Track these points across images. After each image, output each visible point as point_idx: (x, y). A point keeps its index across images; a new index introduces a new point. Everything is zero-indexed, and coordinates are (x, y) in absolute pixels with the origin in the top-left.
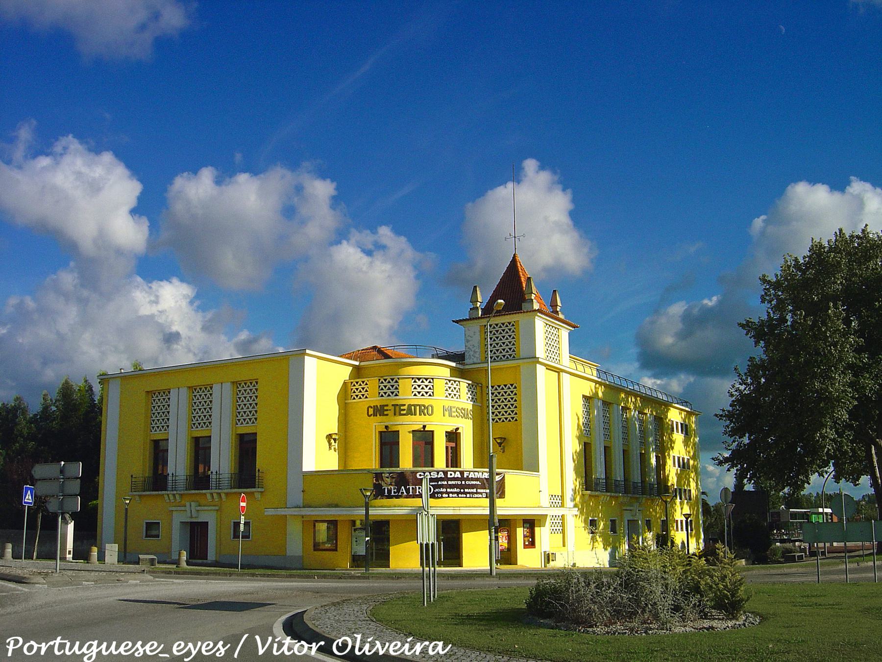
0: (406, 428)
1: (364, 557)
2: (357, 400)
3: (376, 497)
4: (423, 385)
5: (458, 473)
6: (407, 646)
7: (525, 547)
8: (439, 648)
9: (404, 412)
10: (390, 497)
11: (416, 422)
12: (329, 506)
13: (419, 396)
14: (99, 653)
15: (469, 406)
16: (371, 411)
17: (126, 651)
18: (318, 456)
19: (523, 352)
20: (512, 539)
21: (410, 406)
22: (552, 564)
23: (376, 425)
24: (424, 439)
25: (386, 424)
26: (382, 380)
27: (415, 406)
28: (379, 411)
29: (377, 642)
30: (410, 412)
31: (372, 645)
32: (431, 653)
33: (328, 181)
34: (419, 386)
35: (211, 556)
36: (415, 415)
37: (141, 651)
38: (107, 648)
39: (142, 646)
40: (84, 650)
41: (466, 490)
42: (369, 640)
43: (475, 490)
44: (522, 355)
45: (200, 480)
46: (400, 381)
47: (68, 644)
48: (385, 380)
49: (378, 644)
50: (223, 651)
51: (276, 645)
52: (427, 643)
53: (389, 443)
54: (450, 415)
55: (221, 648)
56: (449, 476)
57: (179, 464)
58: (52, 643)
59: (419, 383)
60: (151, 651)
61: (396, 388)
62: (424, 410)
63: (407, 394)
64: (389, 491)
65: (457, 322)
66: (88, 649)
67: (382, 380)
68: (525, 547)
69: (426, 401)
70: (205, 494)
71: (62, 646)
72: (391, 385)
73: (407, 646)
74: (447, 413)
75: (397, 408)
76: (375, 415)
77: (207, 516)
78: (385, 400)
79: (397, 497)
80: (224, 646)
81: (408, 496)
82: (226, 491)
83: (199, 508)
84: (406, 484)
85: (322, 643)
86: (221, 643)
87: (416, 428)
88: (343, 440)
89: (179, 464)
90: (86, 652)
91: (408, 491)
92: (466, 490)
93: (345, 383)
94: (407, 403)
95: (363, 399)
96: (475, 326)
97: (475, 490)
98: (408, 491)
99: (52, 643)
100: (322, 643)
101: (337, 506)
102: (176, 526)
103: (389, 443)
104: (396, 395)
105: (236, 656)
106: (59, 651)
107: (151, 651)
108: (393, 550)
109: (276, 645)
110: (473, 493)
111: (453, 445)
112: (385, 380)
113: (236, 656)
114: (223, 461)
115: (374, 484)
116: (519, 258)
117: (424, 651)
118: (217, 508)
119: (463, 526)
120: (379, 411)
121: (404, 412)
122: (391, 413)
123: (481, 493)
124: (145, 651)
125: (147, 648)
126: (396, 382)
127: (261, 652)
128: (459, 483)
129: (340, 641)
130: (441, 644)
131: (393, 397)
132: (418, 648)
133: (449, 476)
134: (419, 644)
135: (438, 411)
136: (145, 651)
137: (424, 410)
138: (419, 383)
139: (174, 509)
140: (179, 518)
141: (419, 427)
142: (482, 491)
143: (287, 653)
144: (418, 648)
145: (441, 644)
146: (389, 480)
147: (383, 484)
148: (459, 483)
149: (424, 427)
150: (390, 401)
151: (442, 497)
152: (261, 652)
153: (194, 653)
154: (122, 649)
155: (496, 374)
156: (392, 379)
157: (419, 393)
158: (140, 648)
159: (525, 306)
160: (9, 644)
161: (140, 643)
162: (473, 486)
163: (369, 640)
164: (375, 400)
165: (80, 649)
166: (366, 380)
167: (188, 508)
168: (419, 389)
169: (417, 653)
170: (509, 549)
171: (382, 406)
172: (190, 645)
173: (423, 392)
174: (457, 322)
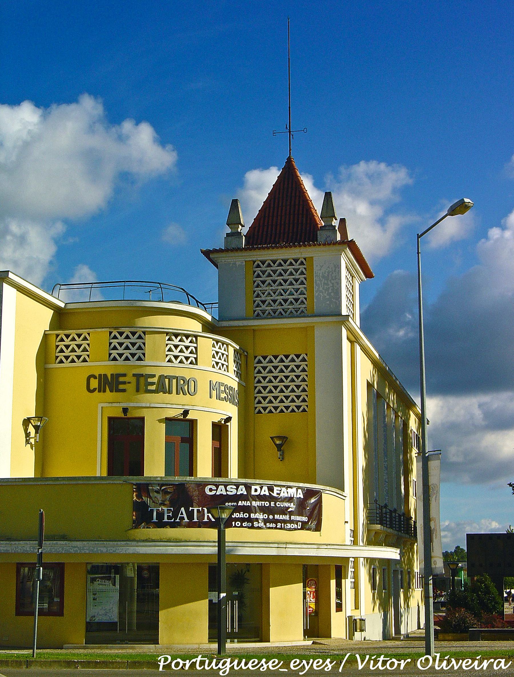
0: (156, 412)
1: (110, 626)
2: (67, 364)
3: (136, 524)
6: (476, 663)
7: (337, 611)
8: (502, 664)
9: (153, 388)
10: (160, 524)
11: (172, 405)
13: (176, 362)
14: (232, 668)
15: (233, 382)
16: (94, 384)
17: (253, 667)
21: (162, 378)
23: (106, 406)
24: (182, 431)
25: (125, 405)
26: (115, 333)
28: (111, 383)
29: (453, 660)
30: (162, 387)
31: (449, 662)
32: (495, 668)
33: (271, 168)
34: (176, 347)
36: (170, 392)
37: (265, 666)
38: (239, 664)
39: (266, 663)
40: (220, 665)
41: (277, 517)
42: (446, 658)
43: (287, 517)
44: (316, 309)
46: (148, 338)
47: (207, 661)
49: (454, 661)
50: (330, 666)
51: (372, 662)
52: (492, 660)
53: (125, 439)
54: (218, 398)
55: (329, 664)
56: (253, 493)
58: (194, 660)
59: (176, 341)
60: (273, 667)
61: (140, 348)
62: (184, 386)
63: (158, 360)
64: (160, 515)
66: (223, 665)
67: (115, 333)
68: (337, 611)
69: (184, 371)
71: (202, 663)
72: (131, 342)
73: (476, 663)
74: (214, 393)
75: (142, 380)
76: (101, 389)
79: (173, 525)
80: (331, 662)
81: (191, 525)
84: (188, 503)
85: (409, 660)
86: (329, 660)
87: (172, 413)
90: (221, 667)
91: (190, 515)
92: (277, 517)
93: (46, 336)
94: (158, 372)
95: (79, 363)
96: (239, 260)
97: (287, 517)
98: (190, 515)
99: (194, 660)
100: (409, 660)
101: (64, 538)
103: (125, 439)
104: (140, 359)
105: (340, 670)
106: (200, 666)
107: (273, 667)
108: (162, 614)
109: (372, 662)
110: (284, 522)
112: (121, 334)
113: (340, 670)
115: (135, 503)
117: (491, 665)
119: (273, 573)
120: (111, 383)
121: (153, 388)
122: (131, 388)
123: (297, 522)
124: (268, 666)
125: (270, 664)
126: (140, 337)
127: (360, 667)
128: (267, 504)
129: (423, 658)
130: (503, 661)
131: (133, 362)
132: (485, 664)
133: (253, 493)
134: (486, 661)
135: (203, 388)
136: (268, 666)
137: (184, 386)
138: (176, 341)
142: (298, 518)
143: (381, 668)
144: (485, 664)
145: (503, 661)
147: (148, 501)
148: (267, 504)
150: (132, 367)
151: (241, 526)
152: (360, 667)
153: (307, 668)
154: (250, 665)
155: (280, 333)
156: (134, 334)
157: (176, 357)
158: (264, 664)
160: (160, 661)
161: (264, 660)
162: (284, 511)
163: (446, 658)
164: (105, 367)
165: (216, 665)
166: (84, 332)
168: (176, 352)
169: (485, 668)
170: (316, 612)
172: (304, 662)
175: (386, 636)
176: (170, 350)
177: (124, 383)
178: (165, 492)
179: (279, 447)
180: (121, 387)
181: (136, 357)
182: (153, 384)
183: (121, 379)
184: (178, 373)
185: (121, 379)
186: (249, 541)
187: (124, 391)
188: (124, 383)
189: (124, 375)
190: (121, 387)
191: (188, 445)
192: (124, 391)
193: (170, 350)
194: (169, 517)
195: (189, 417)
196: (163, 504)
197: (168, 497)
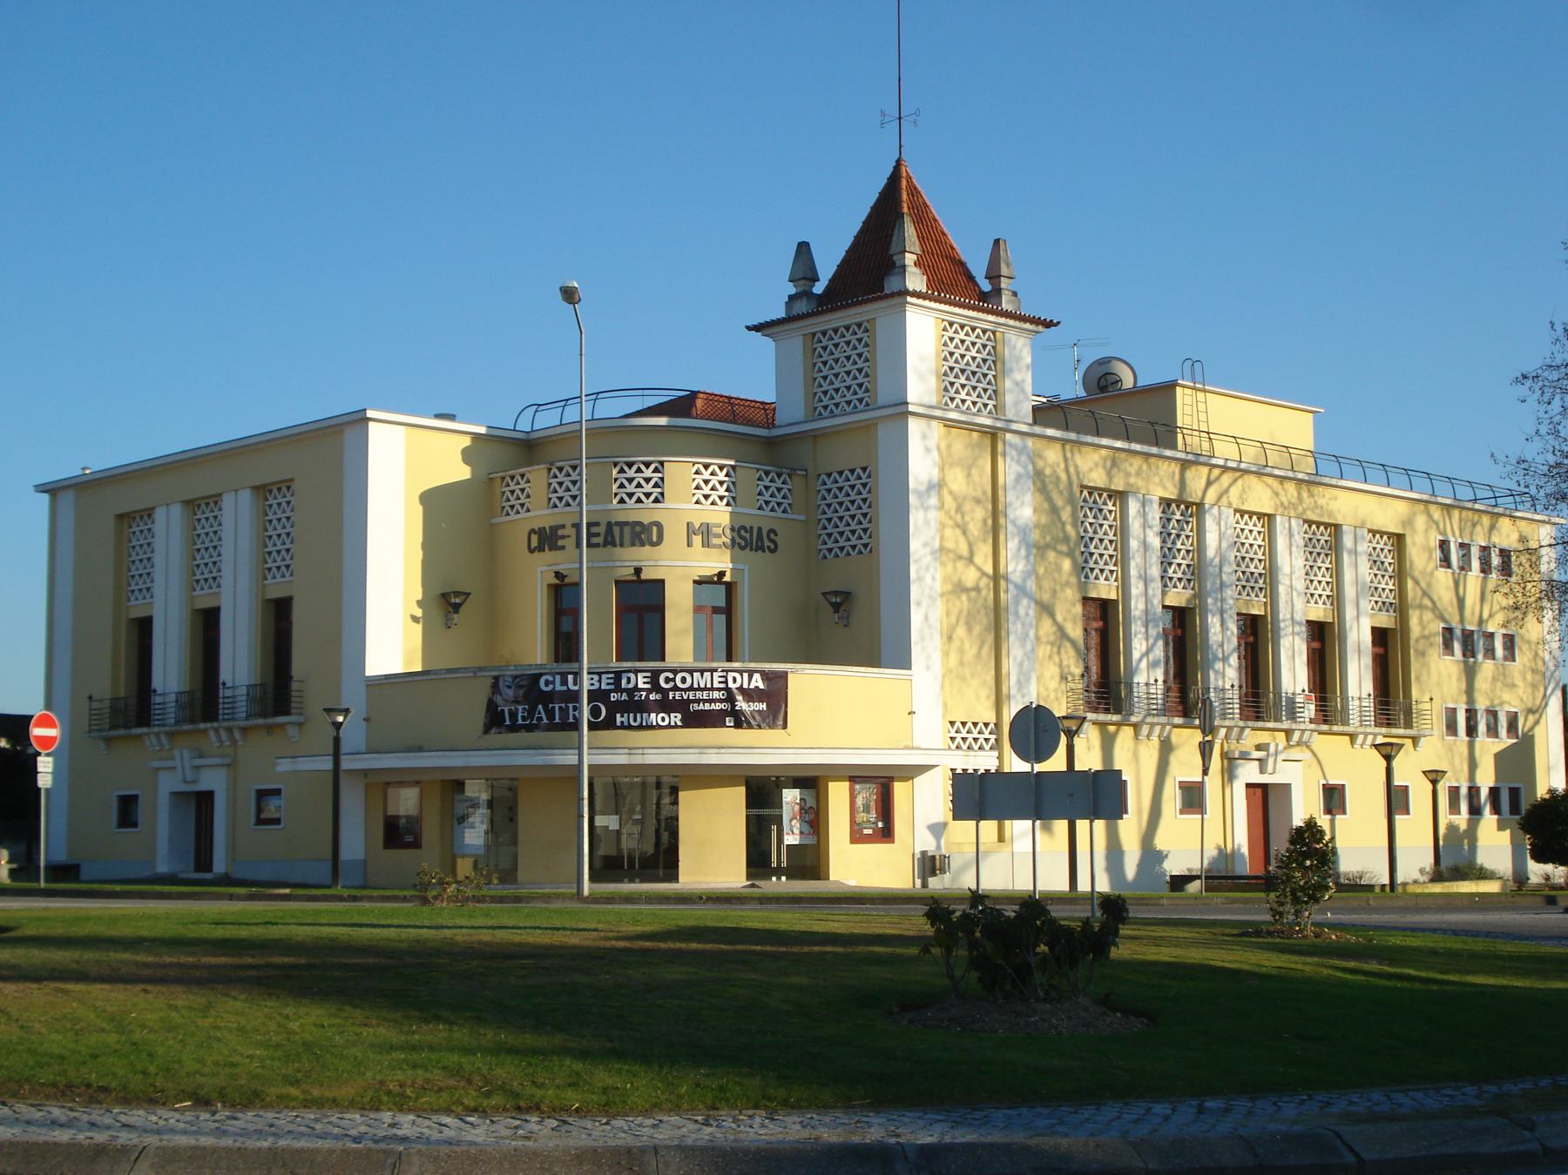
2: (513, 516)
3: (487, 730)
4: (639, 478)
5: (757, 676)
7: (857, 837)
10: (514, 728)
12: (410, 750)
18: (392, 639)
19: (884, 395)
20: (815, 819)
22: (935, 883)
27: (622, 524)
35: (220, 865)
36: (622, 545)
44: (880, 402)
45: (206, 699)
48: (560, 469)
57: (170, 672)
61: (656, 485)
62: (646, 534)
64: (513, 715)
65: (757, 328)
68: (857, 837)
70: (205, 731)
74: (697, 540)
76: (540, 549)
77: (213, 780)
78: (562, 516)
79: (530, 728)
82: (242, 723)
83: (198, 762)
88: (445, 603)
89: (170, 672)
95: (523, 515)
101: (421, 749)
102: (164, 802)
111: (1251, 639)
112: (560, 469)
114: (239, 664)
116: (909, 168)
118: (227, 761)
135: (674, 534)
139: (157, 764)
140: (169, 784)
141: (627, 573)
146: (511, 693)
149: (638, 571)
159: (891, 285)
167: (177, 763)
168: (707, 490)
171: (554, 529)
173: (639, 493)
174: (757, 328)
175: (758, 862)
176: (697, 488)
177: (564, 537)
178: (519, 687)
179: (836, 607)
180: (560, 543)
181: (652, 498)
182: (598, 535)
183: (560, 532)
184: (632, 518)
185: (560, 532)
186: (665, 745)
187: (563, 548)
188: (564, 537)
189: (563, 526)
190: (560, 543)
191: (723, 617)
192: (563, 548)
193: (697, 488)
194: (524, 718)
195: (643, 576)
196: (516, 702)
197: (521, 692)
